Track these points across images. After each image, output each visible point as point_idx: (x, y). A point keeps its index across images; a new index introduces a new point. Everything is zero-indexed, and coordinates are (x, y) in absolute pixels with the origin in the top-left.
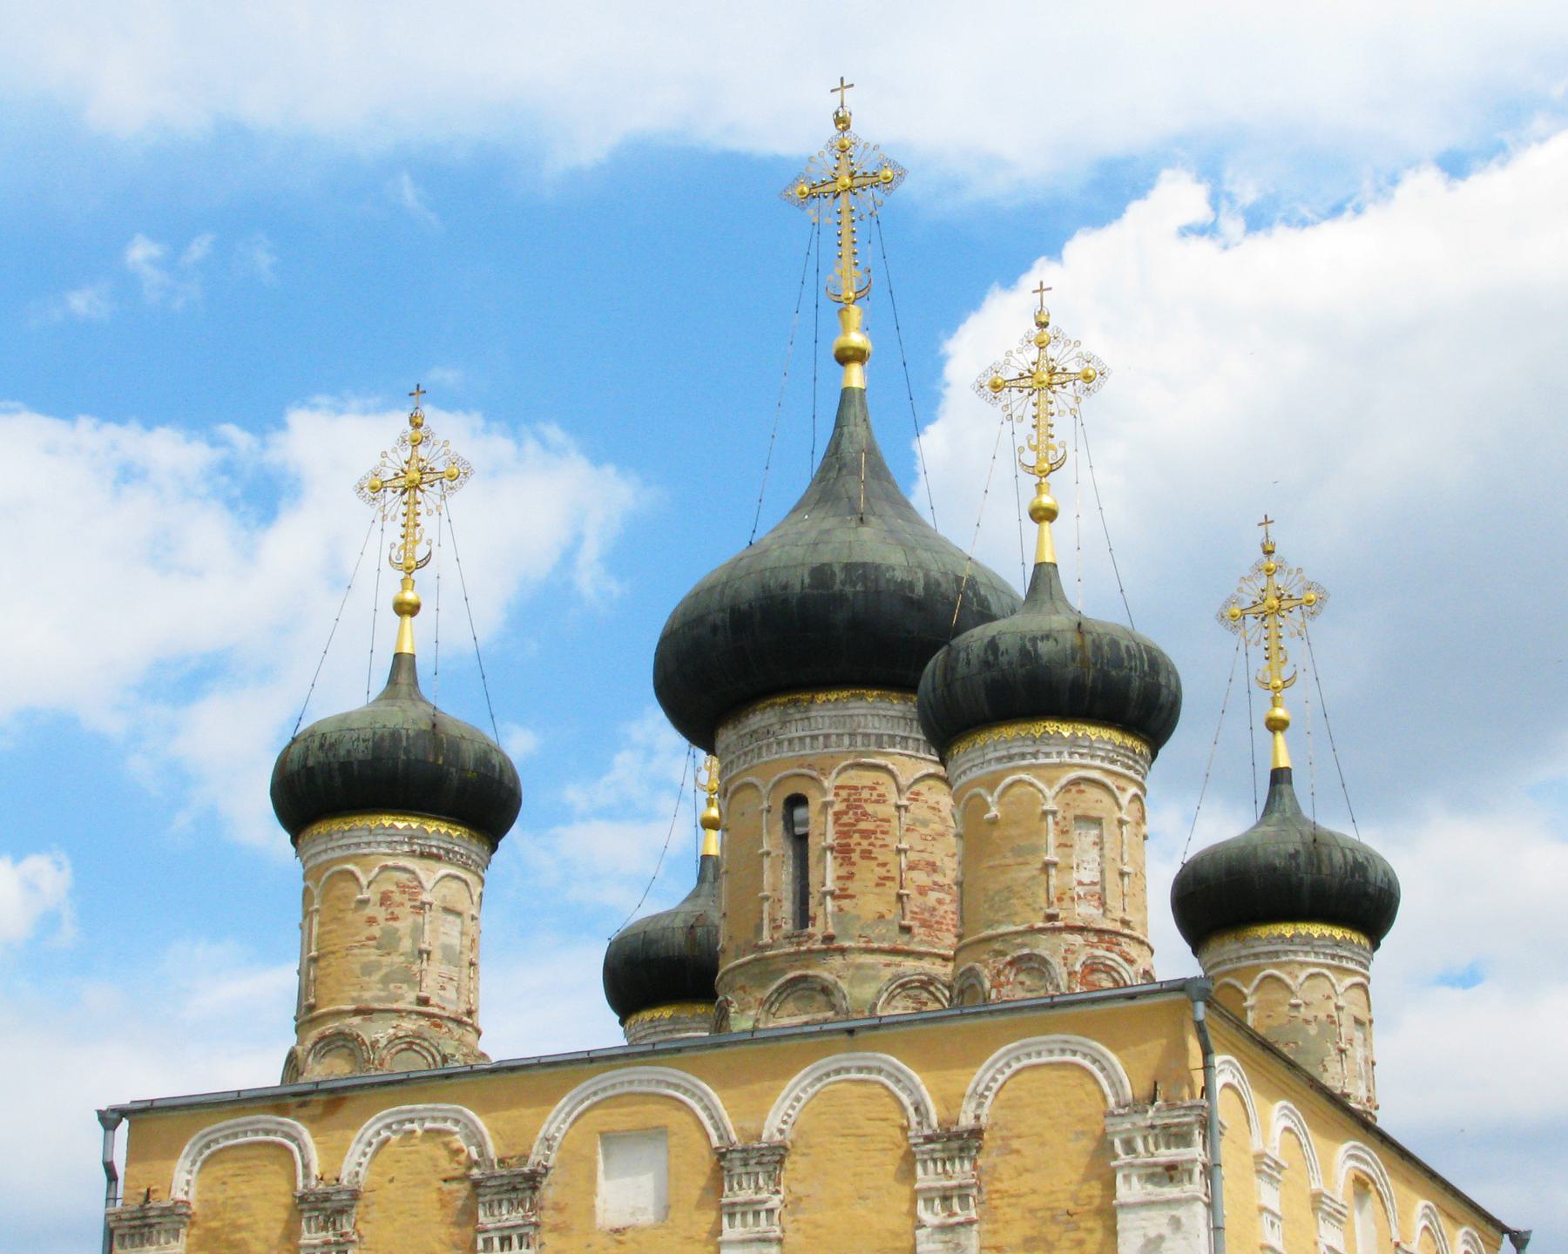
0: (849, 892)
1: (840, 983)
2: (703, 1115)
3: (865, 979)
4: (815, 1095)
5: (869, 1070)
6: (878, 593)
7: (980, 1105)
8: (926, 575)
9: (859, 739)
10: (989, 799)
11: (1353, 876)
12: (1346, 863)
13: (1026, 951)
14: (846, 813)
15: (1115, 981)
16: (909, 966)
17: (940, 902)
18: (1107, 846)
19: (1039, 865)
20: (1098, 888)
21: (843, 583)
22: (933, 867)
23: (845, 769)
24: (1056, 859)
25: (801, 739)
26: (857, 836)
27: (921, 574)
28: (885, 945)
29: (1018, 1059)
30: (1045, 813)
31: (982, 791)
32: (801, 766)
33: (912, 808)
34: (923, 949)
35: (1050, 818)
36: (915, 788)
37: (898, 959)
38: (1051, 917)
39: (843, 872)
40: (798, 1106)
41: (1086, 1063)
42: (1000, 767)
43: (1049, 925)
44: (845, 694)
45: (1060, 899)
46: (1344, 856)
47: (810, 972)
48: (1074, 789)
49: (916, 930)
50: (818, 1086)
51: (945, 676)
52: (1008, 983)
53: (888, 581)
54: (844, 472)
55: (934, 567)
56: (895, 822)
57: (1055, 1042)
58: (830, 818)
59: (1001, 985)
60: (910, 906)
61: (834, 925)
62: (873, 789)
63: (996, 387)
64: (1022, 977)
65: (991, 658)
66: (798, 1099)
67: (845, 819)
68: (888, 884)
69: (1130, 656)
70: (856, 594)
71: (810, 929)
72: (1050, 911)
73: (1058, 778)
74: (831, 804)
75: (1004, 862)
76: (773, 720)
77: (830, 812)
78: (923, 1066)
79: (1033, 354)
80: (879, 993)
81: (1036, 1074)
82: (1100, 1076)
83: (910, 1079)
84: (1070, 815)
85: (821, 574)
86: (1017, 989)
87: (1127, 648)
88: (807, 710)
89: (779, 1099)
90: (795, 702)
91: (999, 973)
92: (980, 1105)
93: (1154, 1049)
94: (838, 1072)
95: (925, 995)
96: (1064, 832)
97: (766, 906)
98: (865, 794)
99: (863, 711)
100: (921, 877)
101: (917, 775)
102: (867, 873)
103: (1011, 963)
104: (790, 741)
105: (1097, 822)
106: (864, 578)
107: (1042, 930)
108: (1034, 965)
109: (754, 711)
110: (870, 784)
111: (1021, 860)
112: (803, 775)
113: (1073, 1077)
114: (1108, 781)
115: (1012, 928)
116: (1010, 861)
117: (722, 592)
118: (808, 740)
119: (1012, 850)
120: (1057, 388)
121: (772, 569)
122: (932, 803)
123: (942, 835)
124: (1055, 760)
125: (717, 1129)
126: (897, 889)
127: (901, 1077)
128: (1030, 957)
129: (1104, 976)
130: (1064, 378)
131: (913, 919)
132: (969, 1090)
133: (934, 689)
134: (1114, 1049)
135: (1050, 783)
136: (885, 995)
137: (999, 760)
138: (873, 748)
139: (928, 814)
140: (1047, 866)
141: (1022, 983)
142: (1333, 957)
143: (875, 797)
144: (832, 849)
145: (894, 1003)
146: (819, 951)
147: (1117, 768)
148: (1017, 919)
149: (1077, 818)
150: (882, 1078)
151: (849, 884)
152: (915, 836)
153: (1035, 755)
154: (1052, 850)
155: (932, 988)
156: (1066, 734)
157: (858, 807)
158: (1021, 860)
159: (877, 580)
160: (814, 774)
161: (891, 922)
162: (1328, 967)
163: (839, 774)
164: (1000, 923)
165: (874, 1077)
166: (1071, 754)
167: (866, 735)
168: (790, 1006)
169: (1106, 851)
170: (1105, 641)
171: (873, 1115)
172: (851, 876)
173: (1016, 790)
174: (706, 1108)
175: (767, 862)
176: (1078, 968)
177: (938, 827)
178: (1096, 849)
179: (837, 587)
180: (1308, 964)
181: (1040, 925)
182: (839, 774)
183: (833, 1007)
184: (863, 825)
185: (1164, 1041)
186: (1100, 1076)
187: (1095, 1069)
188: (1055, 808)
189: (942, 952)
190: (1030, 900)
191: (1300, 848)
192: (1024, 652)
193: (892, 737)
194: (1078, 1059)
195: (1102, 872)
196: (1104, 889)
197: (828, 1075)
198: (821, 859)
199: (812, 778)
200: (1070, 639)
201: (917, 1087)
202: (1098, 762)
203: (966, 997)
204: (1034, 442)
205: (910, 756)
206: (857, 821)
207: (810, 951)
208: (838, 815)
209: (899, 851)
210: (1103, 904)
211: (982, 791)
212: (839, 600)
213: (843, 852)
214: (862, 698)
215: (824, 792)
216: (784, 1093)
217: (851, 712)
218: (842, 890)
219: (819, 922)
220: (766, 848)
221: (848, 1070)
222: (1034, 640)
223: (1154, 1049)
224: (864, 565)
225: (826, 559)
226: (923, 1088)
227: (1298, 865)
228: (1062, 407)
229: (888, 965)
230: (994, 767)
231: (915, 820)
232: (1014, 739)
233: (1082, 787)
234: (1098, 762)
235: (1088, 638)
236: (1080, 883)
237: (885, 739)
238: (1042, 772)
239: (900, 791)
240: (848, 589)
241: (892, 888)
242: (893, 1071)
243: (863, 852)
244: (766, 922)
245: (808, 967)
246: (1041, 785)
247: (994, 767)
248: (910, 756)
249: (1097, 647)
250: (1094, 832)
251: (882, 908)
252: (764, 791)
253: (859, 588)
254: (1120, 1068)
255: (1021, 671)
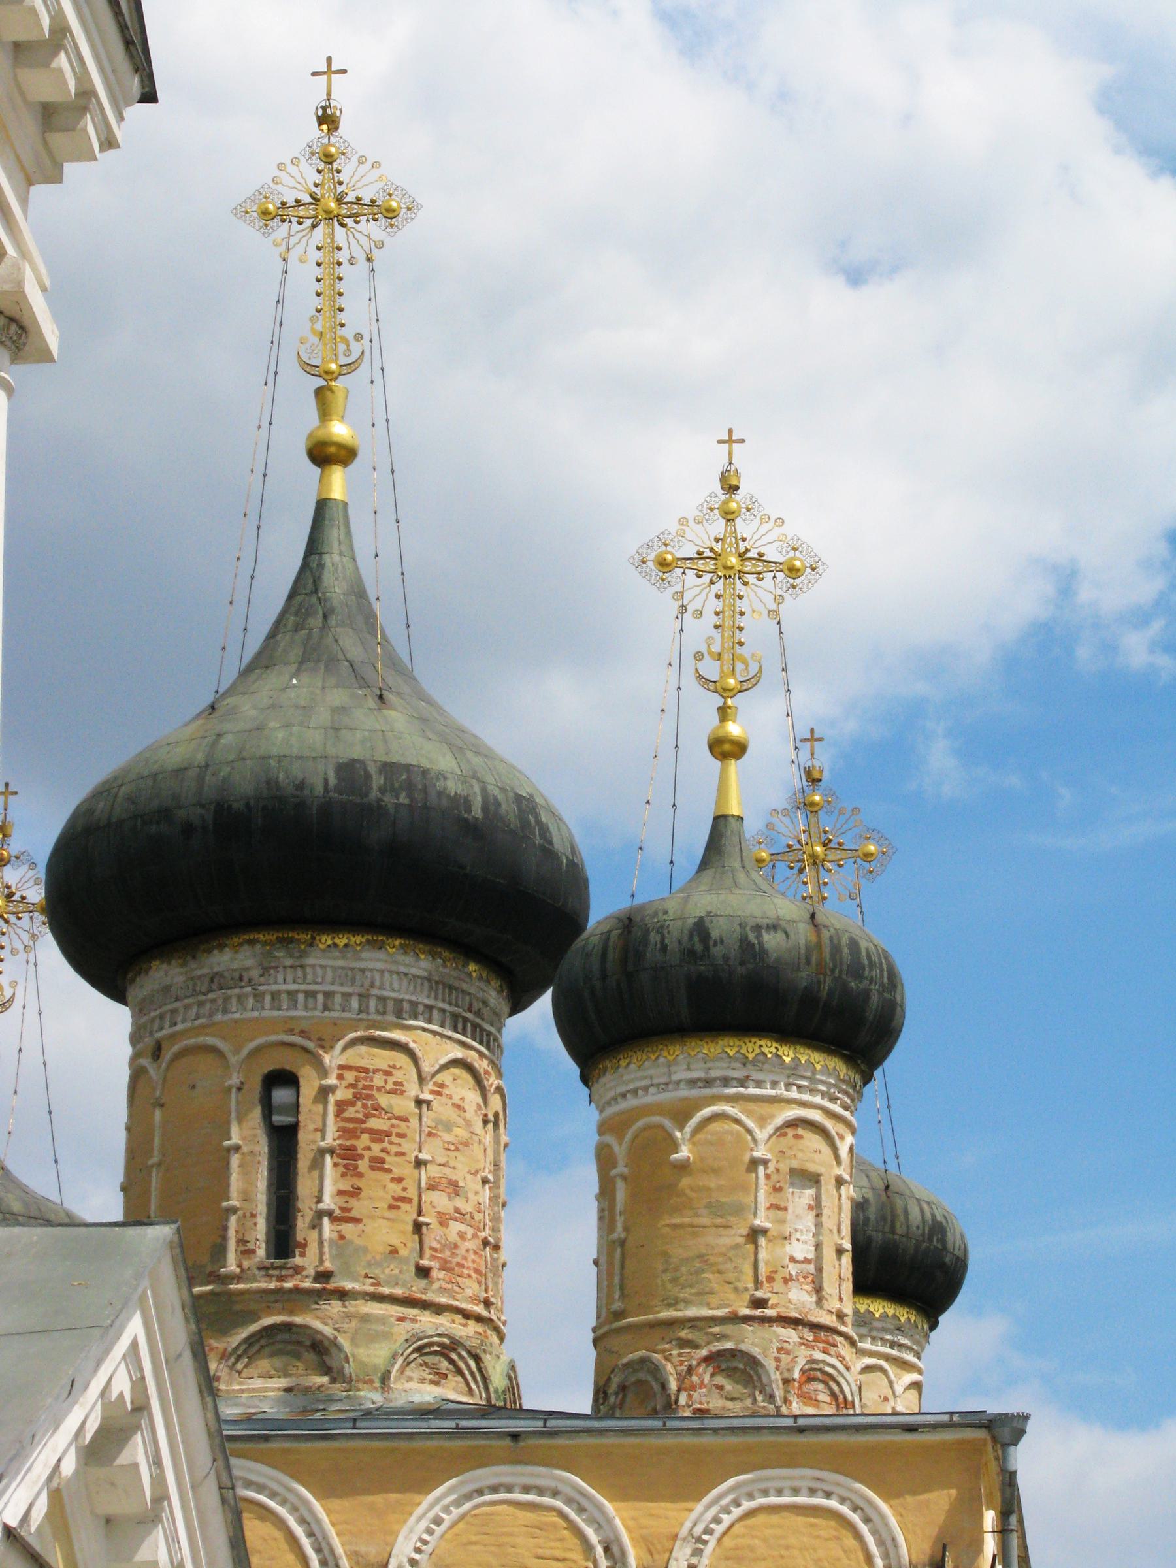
0: (354, 1214)
1: (341, 1340)
2: (299, 1531)
3: (374, 1338)
4: (462, 1517)
5: (541, 1491)
6: (426, 808)
7: (697, 1552)
8: (484, 790)
9: (372, 1003)
10: (678, 1134)
11: (930, 1240)
12: (924, 1221)
13: (729, 1345)
14: (353, 1104)
15: (833, 1395)
16: (427, 1322)
17: (462, 1236)
18: (825, 1212)
19: (745, 1232)
20: (811, 1268)
21: (382, 790)
22: (455, 1188)
23: (354, 1043)
24: (767, 1225)
25: (292, 994)
26: (365, 1137)
27: (477, 789)
28: (399, 1291)
29: (751, 1497)
30: (754, 1163)
31: (667, 1123)
32: (291, 1031)
33: (435, 1104)
34: (443, 1300)
35: (761, 1169)
36: (439, 1078)
37: (412, 1312)
38: (759, 1303)
39: (345, 1185)
40: (439, 1531)
41: (845, 1510)
42: (695, 1093)
43: (758, 1312)
44: (359, 939)
45: (770, 1279)
46: (922, 1211)
47: (298, 1320)
48: (790, 1132)
49: (435, 1274)
50: (467, 1506)
51: (624, 961)
52: (702, 1385)
53: (440, 794)
54: (332, 621)
55: (490, 779)
56: (414, 1122)
57: (802, 1478)
58: (331, 1108)
59: (693, 1388)
60: (431, 1240)
61: (332, 1258)
62: (387, 1073)
63: (664, 565)
64: (720, 1380)
65: (699, 947)
66: (438, 1521)
67: (350, 1112)
68: (405, 1207)
69: (872, 964)
70: (398, 806)
71: (298, 1260)
72: (759, 1294)
73: (772, 1116)
74: (330, 1089)
75: (697, 1221)
76: (249, 963)
77: (332, 1099)
78: (620, 1494)
79: (719, 526)
80: (394, 1356)
81: (774, 1519)
82: (864, 1529)
83: (600, 1508)
84: (784, 1167)
85: (350, 771)
86: (710, 1394)
87: (867, 949)
88: (303, 954)
89: (413, 1519)
90: (286, 942)
91: (690, 1370)
92: (697, 1552)
93: (941, 1500)
94: (495, 1489)
95: (445, 1364)
96: (777, 1190)
97: (233, 1220)
98: (378, 1080)
99: (379, 965)
100: (439, 1201)
101: (443, 1061)
102: (377, 1190)
103: (707, 1360)
104: (275, 996)
105: (814, 1180)
106: (409, 786)
107: (747, 1319)
108: (741, 1368)
109: (221, 947)
110: (385, 1067)
111: (718, 1221)
112: (292, 1045)
113: (827, 1528)
114: (829, 1124)
115: (705, 1312)
116: (705, 1221)
117: (201, 778)
118: (301, 997)
119: (708, 1206)
120: (750, 578)
121: (280, 758)
122: (456, 1100)
123: (466, 1144)
124: (768, 1091)
125: (318, 1550)
126: (415, 1216)
127: (585, 1503)
128: (734, 1354)
129: (821, 1386)
130: (760, 566)
131: (433, 1258)
132: (684, 1532)
133: (604, 977)
134: (886, 1497)
135: (762, 1121)
136: (400, 1361)
137: (692, 1083)
138: (390, 1018)
139: (450, 1114)
140: (755, 1234)
141: (721, 1388)
142: (893, 1345)
143: (389, 1086)
144: (332, 1152)
145: (408, 1372)
146: (309, 1292)
147: (836, 1108)
148: (714, 1301)
149: (793, 1171)
150: (558, 1503)
151: (353, 1202)
152: (437, 1142)
153: (742, 1083)
154: (762, 1212)
155: (454, 1356)
156: (787, 1060)
157: (368, 1097)
158: (718, 1221)
159: (425, 790)
160: (310, 1045)
161: (406, 1260)
162: (887, 1358)
163: (345, 1048)
164: (687, 1302)
165: (547, 1500)
166: (788, 1086)
167: (383, 999)
168: (264, 1364)
169: (824, 1219)
170: (845, 941)
171: (547, 1553)
172: (356, 1192)
173: (715, 1127)
174: (302, 1521)
175: (235, 1160)
176: (796, 1375)
177: (461, 1132)
178: (812, 1214)
179: (374, 794)
180: (871, 1354)
181: (747, 1311)
182: (345, 1048)
183: (326, 1370)
184: (374, 1123)
185: (954, 1492)
186: (864, 1529)
187: (855, 1518)
188: (769, 1156)
189: (464, 1306)
190: (731, 1276)
191: (869, 1195)
192: (745, 946)
193: (414, 1004)
194: (833, 1503)
195: (818, 1246)
196: (819, 1270)
197: (480, 1492)
198: (317, 1164)
199: (305, 1050)
200: (803, 934)
201: (610, 1521)
202: (817, 1099)
203: (630, 1397)
204: (716, 648)
205: (435, 1033)
206: (367, 1116)
207: (297, 1290)
208: (341, 1106)
209: (419, 1163)
210: (818, 1290)
211: (667, 1123)
212: (375, 811)
213: (348, 1157)
214: (381, 946)
215: (323, 1072)
216: (419, 1511)
217: (362, 965)
218: (342, 1209)
219: (312, 1250)
220: (235, 1139)
221: (509, 1489)
222: (758, 928)
223: (941, 1500)
224: (408, 768)
225: (357, 753)
226: (618, 1522)
227: (867, 1220)
228: (757, 605)
229: (401, 1319)
230: (684, 1092)
231: (439, 1122)
232: (718, 1058)
233: (800, 1131)
234: (817, 1099)
235: (826, 935)
236: (792, 1259)
237: (421, 1008)
238: (752, 1106)
239: (421, 1079)
240: (388, 799)
241: (408, 1213)
242: (573, 1494)
243: (373, 1159)
244: (232, 1244)
245: (291, 1313)
246: (750, 1124)
247: (684, 1092)
248: (435, 1033)
249: (836, 949)
250: (810, 1192)
251: (396, 1241)
252: (233, 1060)
253: (403, 799)
254: (893, 1521)
255: (741, 970)
